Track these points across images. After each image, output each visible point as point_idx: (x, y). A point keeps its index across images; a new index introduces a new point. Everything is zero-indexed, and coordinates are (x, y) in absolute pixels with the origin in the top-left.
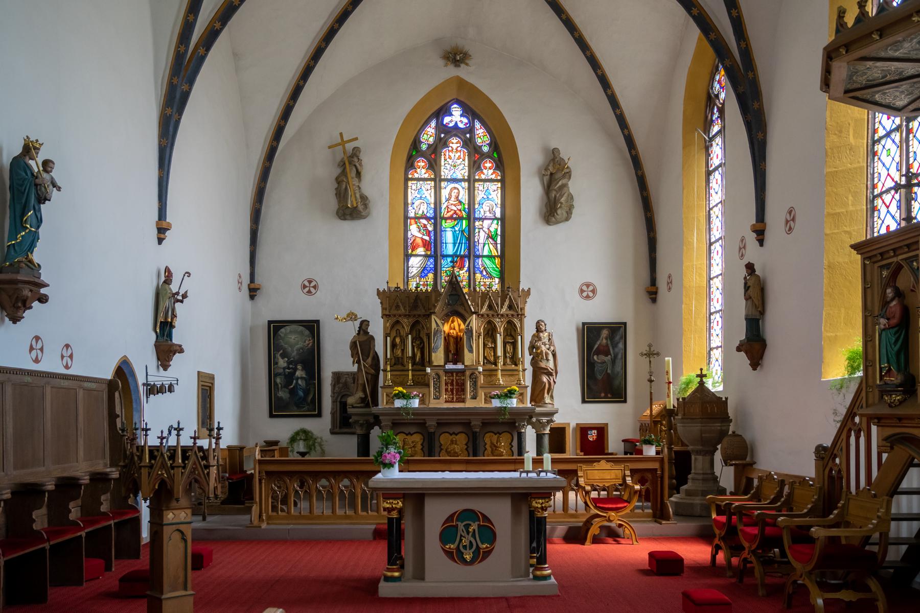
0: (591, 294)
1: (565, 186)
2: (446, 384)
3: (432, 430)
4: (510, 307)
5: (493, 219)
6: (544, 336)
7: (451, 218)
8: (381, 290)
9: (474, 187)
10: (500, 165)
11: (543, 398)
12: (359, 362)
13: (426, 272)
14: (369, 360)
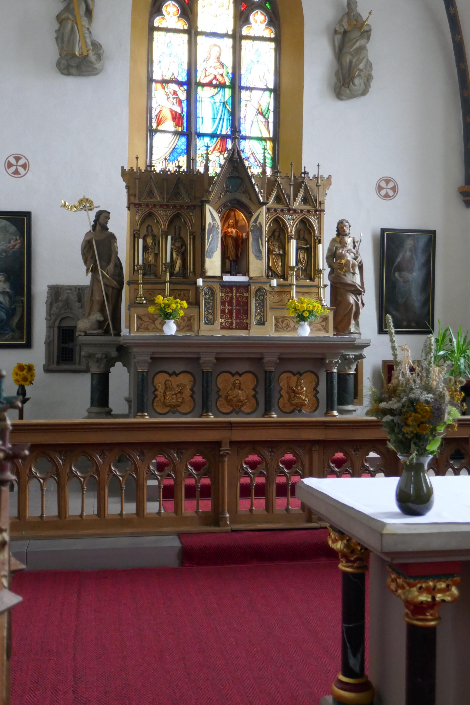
0: (391, 193)
1: (362, 48)
2: (223, 303)
3: (209, 369)
4: (305, 200)
5: (264, 90)
6: (349, 240)
7: (210, 84)
8: (127, 168)
9: (240, 46)
10: (274, 20)
11: (349, 324)
12: (94, 270)
13: (175, 154)
14: (111, 267)
